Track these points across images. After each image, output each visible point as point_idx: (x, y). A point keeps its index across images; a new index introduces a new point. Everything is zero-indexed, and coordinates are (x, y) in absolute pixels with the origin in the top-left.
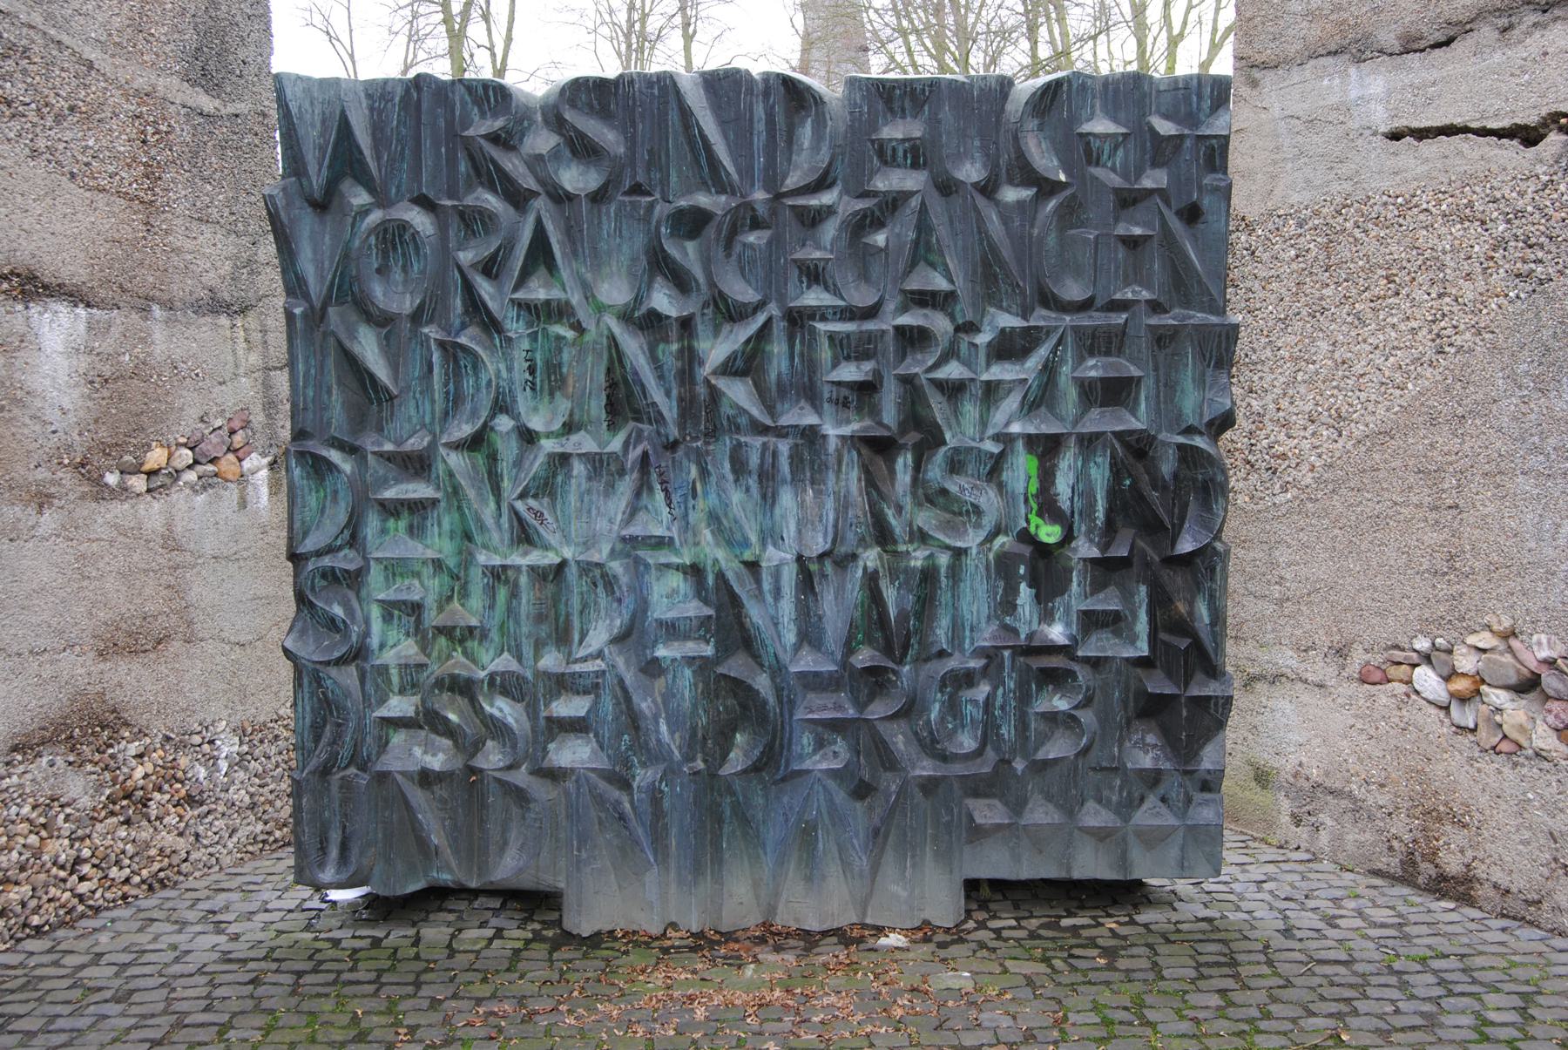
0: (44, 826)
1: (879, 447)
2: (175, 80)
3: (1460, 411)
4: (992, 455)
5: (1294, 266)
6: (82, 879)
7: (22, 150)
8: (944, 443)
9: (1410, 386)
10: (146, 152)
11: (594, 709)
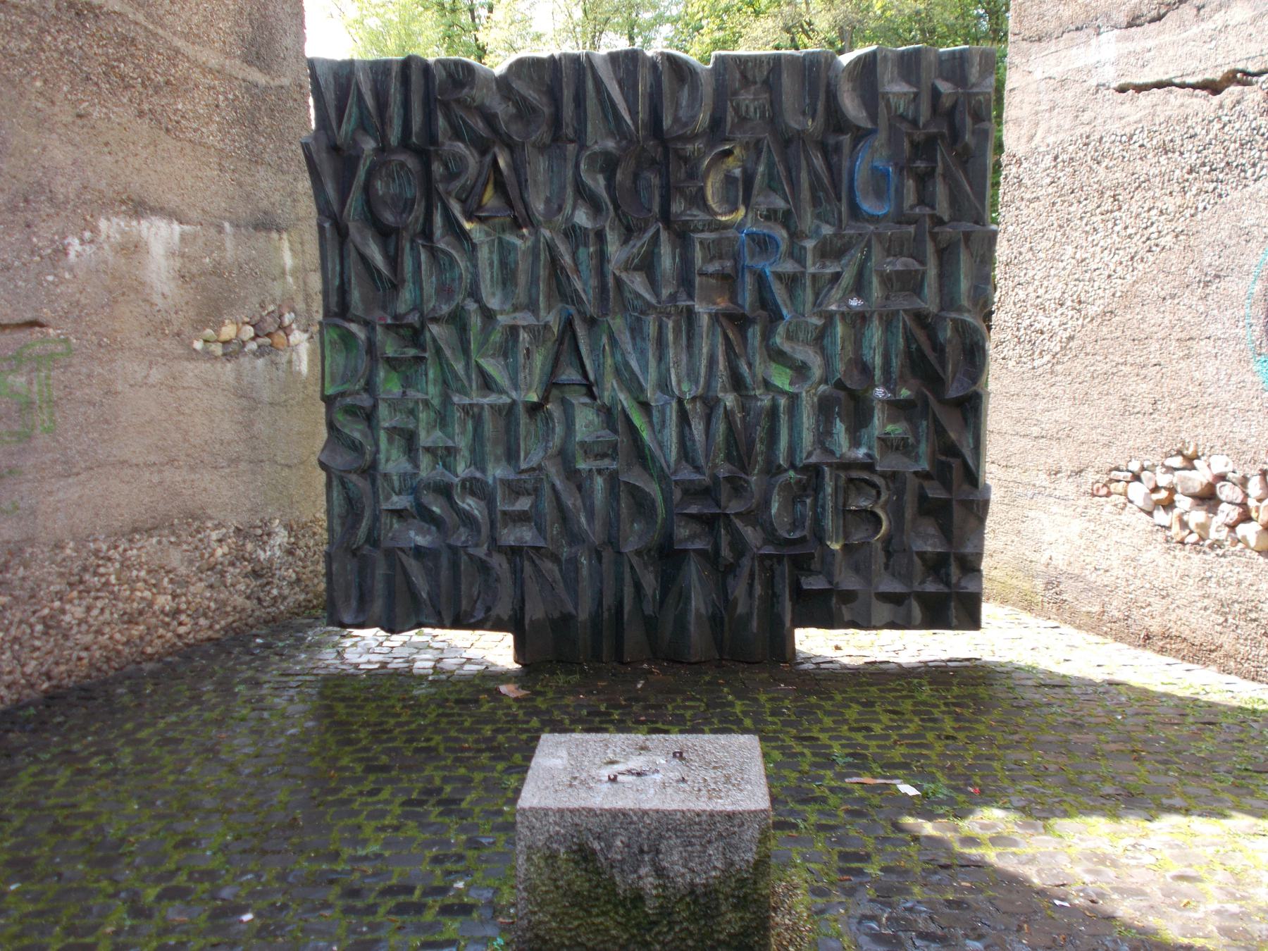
0: (154, 585)
1: (739, 321)
2: (238, 62)
3: (1162, 294)
4: (816, 327)
5: (1050, 190)
6: (181, 624)
7: (132, 110)
8: (782, 318)
9: (1128, 276)
10: (219, 115)
11: (535, 505)
